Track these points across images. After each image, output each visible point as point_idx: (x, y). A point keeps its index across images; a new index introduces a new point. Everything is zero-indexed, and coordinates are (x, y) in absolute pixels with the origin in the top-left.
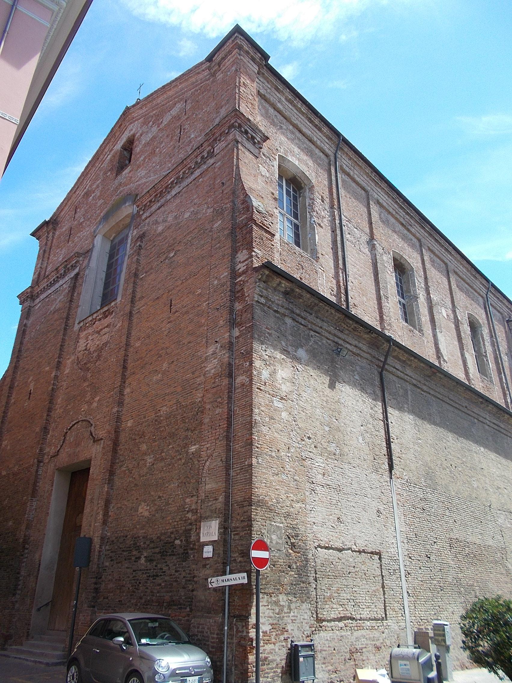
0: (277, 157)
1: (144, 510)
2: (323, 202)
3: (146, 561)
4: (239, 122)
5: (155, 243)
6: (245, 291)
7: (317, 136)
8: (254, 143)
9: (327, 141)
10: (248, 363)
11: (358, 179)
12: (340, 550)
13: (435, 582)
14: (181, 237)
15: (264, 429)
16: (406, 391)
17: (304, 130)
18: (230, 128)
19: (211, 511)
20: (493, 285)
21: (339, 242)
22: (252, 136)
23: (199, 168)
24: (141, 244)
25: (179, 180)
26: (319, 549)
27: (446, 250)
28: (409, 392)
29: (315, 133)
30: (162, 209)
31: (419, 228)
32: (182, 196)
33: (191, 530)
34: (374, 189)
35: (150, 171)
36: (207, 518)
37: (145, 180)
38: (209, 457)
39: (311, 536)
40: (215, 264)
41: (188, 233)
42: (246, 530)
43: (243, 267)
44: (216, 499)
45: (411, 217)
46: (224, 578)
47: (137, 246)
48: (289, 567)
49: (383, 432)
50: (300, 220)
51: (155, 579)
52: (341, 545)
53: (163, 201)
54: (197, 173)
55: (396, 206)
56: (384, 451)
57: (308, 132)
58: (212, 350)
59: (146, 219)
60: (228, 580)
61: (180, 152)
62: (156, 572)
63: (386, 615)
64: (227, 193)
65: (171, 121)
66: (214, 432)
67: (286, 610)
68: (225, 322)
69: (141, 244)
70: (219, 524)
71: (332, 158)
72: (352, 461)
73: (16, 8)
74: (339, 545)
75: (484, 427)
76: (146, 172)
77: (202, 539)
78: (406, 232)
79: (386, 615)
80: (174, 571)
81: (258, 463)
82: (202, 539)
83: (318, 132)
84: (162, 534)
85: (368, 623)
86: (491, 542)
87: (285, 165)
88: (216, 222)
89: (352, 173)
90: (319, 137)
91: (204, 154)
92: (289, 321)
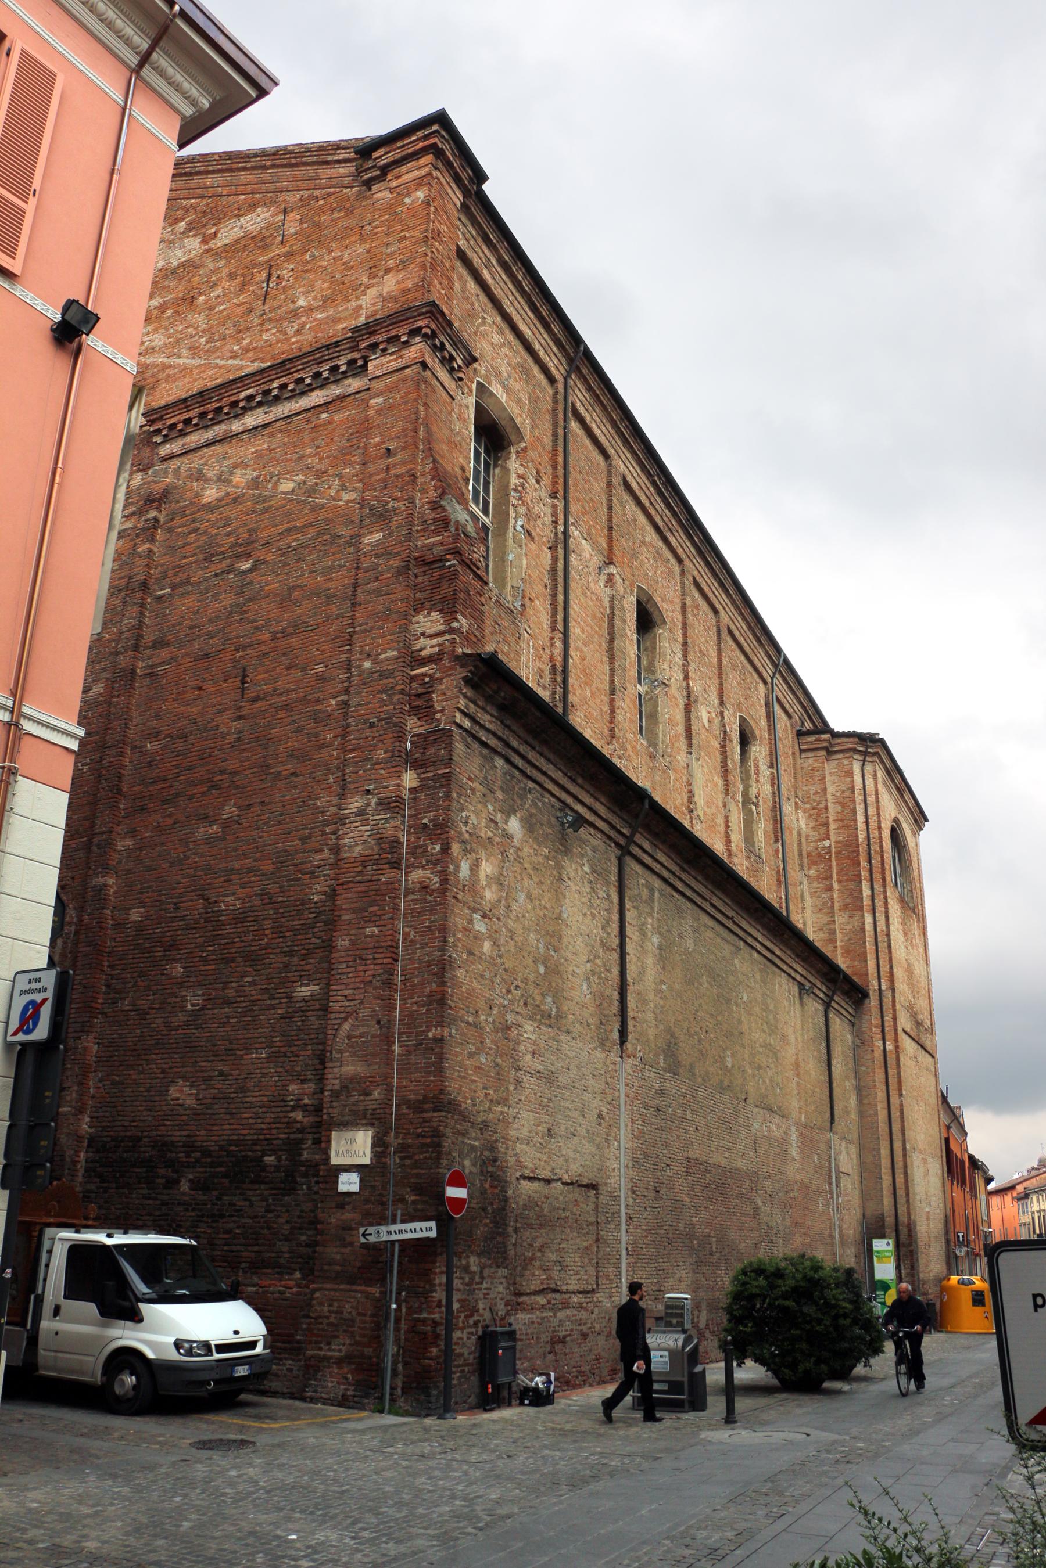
0: (474, 386)
1: (182, 1093)
2: (538, 482)
3: (191, 1189)
4: (434, 327)
5: (198, 525)
6: (435, 699)
7: (540, 340)
8: (451, 371)
9: (555, 349)
10: (438, 848)
11: (597, 431)
12: (548, 1182)
13: (663, 1232)
14: (272, 531)
15: (460, 973)
16: (652, 890)
17: (522, 327)
18: (414, 332)
19: (354, 1113)
20: (786, 662)
21: (560, 573)
22: (451, 355)
23: (321, 387)
24: (158, 515)
25: (269, 399)
26: (522, 1182)
27: (722, 585)
28: (657, 894)
29: (538, 335)
30: (218, 449)
31: (684, 537)
32: (272, 435)
33: (301, 1141)
34: (621, 454)
35: (178, 341)
36: (345, 1125)
37: (166, 360)
38: (349, 1014)
39: (512, 1161)
40: (366, 624)
41: (289, 530)
42: (427, 1152)
43: (432, 647)
44: (367, 1095)
45: (674, 514)
46: (393, 1228)
47: (148, 520)
48: (483, 1209)
49: (616, 971)
50: (493, 516)
51: (217, 1221)
52: (550, 1174)
53: (219, 430)
54: (316, 397)
55: (652, 489)
56: (615, 1008)
57: (527, 333)
58: (356, 805)
59: (171, 457)
60: (400, 1232)
61: (265, 327)
62: (218, 1210)
63: (598, 1285)
64: (397, 476)
65: (243, 242)
66: (361, 968)
67: (477, 1279)
68: (390, 754)
69: (158, 515)
70: (373, 1137)
71: (560, 386)
72: (571, 1029)
73: (130, 114)
74: (546, 1174)
75: (751, 956)
76: (167, 341)
77: (335, 1160)
78: (660, 544)
79: (598, 1285)
80: (263, 1210)
81: (450, 1036)
82: (335, 1160)
83: (542, 330)
84: (231, 1143)
85: (575, 1299)
86: (740, 1164)
87: (488, 404)
88: (371, 533)
89: (588, 419)
90: (542, 341)
91: (340, 363)
92: (499, 762)
